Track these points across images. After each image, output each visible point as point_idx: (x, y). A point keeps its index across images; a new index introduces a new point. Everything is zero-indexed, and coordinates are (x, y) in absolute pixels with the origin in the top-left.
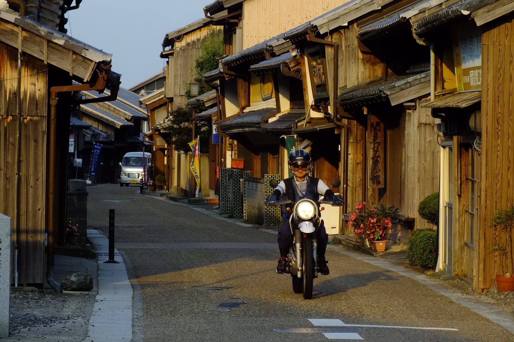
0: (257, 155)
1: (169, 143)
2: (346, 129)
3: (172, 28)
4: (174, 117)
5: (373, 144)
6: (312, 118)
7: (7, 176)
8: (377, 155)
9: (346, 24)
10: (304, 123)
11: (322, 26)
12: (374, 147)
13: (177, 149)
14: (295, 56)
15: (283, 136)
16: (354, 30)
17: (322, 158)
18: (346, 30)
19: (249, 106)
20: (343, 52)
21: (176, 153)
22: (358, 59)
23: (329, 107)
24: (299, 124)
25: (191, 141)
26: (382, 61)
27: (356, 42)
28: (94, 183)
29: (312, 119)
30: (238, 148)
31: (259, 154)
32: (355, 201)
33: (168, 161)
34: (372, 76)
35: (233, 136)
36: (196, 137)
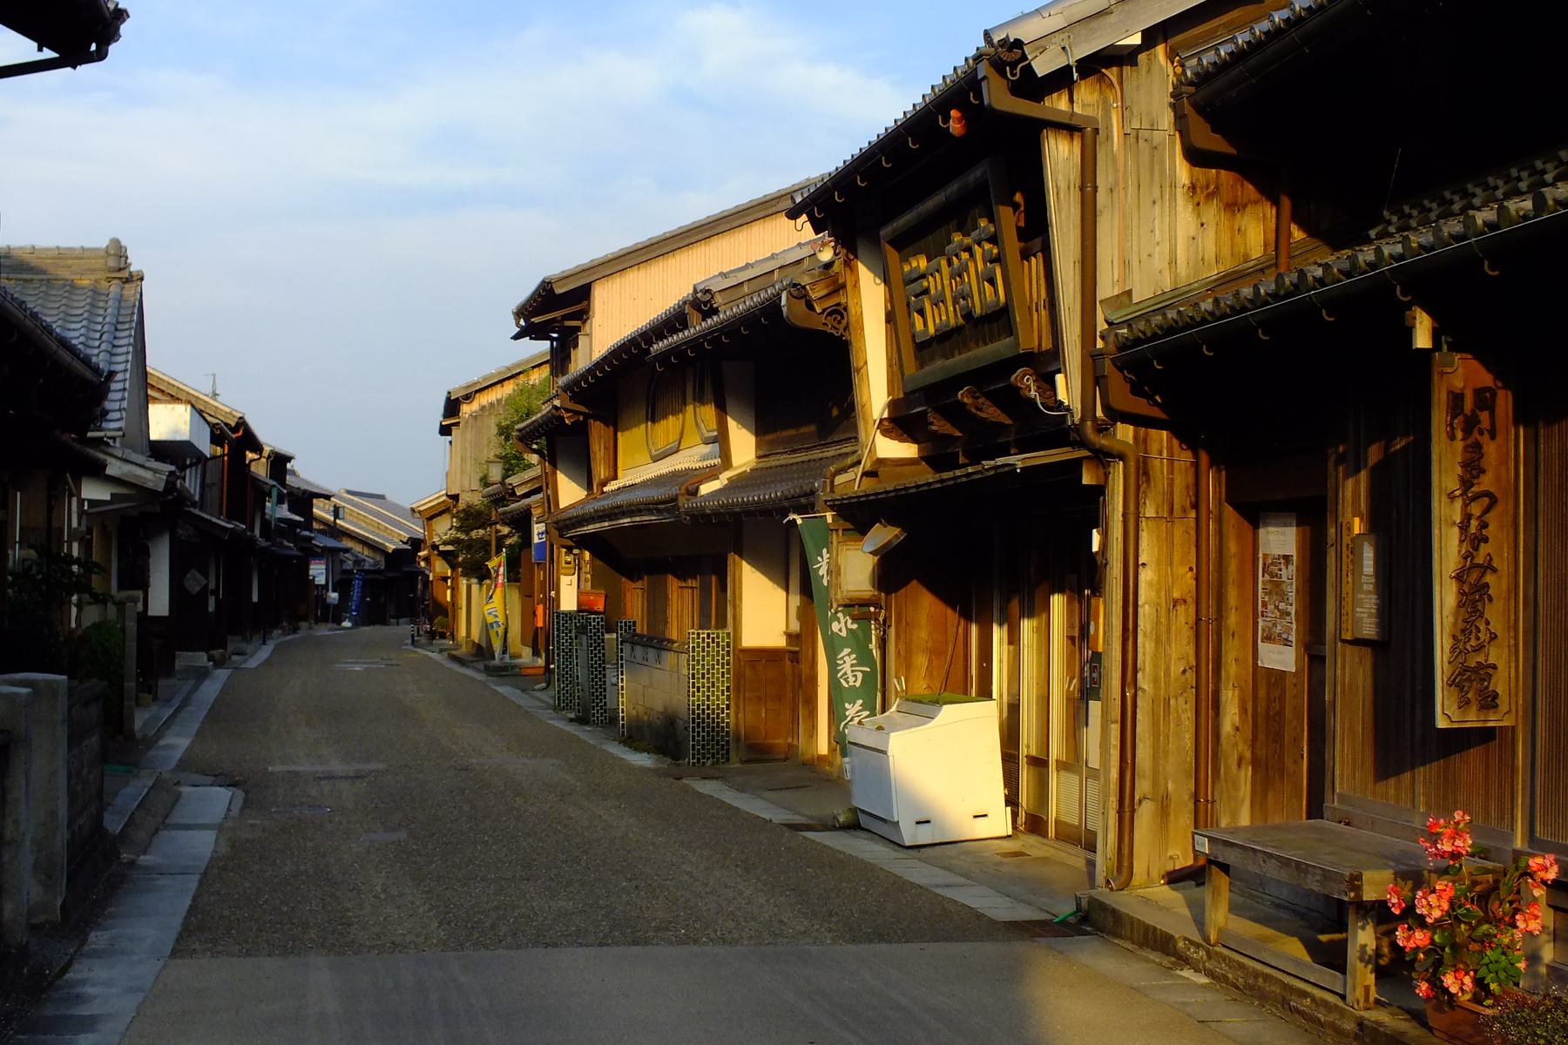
0: (632, 580)
1: (453, 568)
2: (1132, 464)
3: (457, 382)
4: (460, 519)
5: (1458, 504)
6: (882, 461)
7: (1193, 514)
8: (1480, 560)
9: (1136, 40)
10: (855, 474)
11: (1041, 42)
12: (1467, 517)
13: (464, 575)
14: (829, 265)
15: (792, 516)
16: (1155, 70)
17: (915, 582)
18: (1127, 69)
19: (615, 478)
20: (1114, 159)
21: (463, 582)
22: (1173, 186)
23: (1059, 378)
24: (839, 480)
25: (489, 559)
26: (1270, 193)
27: (1166, 119)
28: (356, 625)
29: (882, 462)
30: (593, 568)
31: (640, 578)
32: (1166, 752)
33: (453, 596)
34: (1226, 251)
35: (584, 542)
36: (498, 552)
